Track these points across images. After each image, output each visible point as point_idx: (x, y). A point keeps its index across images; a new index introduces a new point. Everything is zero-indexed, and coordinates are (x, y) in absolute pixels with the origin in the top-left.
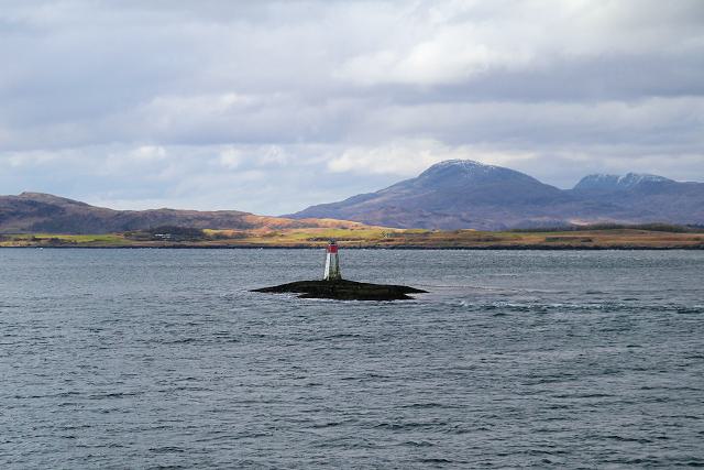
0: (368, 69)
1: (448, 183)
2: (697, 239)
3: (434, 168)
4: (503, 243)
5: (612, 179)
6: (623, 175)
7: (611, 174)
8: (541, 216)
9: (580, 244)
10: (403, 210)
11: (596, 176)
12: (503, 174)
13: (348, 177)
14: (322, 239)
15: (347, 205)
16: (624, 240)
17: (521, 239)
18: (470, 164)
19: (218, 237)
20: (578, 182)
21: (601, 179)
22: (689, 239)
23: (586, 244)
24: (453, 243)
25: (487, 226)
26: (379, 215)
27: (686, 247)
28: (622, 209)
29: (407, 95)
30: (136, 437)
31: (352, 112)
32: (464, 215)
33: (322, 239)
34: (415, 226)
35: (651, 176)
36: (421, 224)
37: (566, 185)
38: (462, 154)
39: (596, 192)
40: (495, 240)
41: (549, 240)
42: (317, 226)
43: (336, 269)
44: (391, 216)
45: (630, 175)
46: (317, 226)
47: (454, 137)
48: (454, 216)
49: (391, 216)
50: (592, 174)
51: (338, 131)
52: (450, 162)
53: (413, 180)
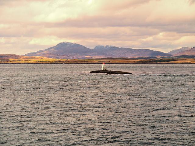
0: (40, 18)
1: (62, 48)
2: (134, 61)
3: (59, 44)
4: (88, 62)
5: (103, 47)
6: (105, 46)
7: (103, 45)
8: (87, 56)
9: (108, 62)
10: (53, 54)
11: (99, 46)
12: (77, 45)
13: (35, 46)
14: (40, 61)
15: (39, 52)
16: (117, 62)
17: (156, 57)
18: (69, 43)
19: (13, 61)
20: (95, 47)
21: (100, 47)
22: (132, 61)
23: (109, 62)
24: (66, 62)
25: (74, 58)
26: (47, 55)
27: (132, 63)
28: (106, 54)
29: (49, 25)
30: (59, 115)
31: (34, 31)
32: (69, 55)
33: (40, 61)
34: (56, 58)
35: (112, 46)
36: (58, 58)
37: (92, 48)
38: (72, 41)
39: (99, 50)
40: (86, 61)
41: (99, 61)
42: (35, 58)
43: (105, 68)
44: (51, 55)
45: (107, 46)
46: (35, 58)
47: (60, 36)
48: (66, 56)
49: (51, 55)
50: (98, 45)
51: (31, 34)
52: (64, 42)
53: (55, 47)
